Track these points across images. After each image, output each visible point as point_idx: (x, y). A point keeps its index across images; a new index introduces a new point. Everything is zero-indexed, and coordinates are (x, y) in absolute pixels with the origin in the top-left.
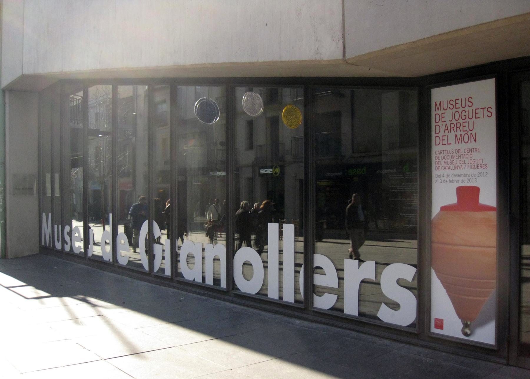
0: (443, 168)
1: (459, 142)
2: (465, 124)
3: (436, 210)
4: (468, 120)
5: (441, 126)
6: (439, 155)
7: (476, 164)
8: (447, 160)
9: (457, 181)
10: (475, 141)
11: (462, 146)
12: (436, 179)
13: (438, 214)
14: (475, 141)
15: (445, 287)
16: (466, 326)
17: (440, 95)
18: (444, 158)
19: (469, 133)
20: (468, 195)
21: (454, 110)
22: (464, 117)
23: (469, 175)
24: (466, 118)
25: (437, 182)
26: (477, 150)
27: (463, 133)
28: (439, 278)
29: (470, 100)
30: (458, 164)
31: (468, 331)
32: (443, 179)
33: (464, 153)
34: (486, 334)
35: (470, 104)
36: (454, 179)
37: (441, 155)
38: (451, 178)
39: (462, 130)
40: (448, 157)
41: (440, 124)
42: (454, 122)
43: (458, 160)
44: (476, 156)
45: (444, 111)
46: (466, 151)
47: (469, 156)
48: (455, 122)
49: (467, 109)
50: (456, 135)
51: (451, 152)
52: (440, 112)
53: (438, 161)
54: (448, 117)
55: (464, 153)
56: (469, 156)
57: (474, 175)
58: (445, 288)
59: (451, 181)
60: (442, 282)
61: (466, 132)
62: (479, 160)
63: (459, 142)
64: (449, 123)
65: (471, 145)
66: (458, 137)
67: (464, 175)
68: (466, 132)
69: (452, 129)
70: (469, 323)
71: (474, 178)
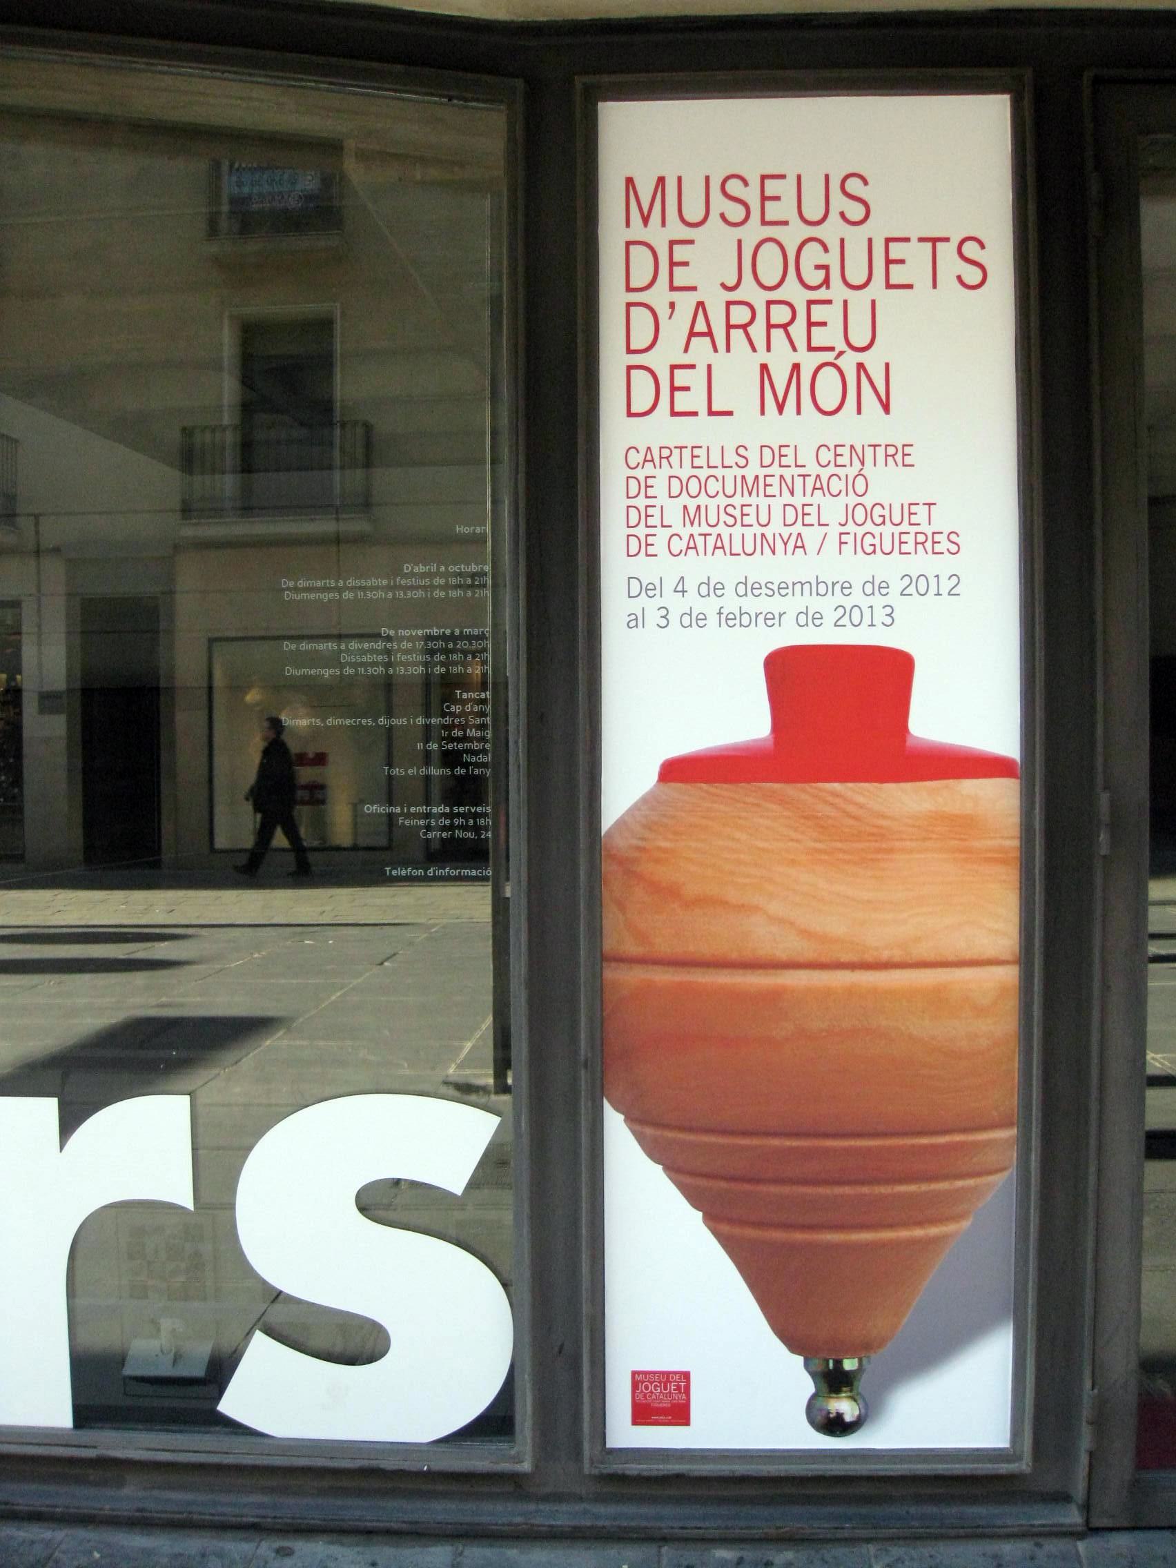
0: (677, 545)
1: (781, 408)
2: (818, 313)
3: (627, 779)
4: (837, 291)
5: (663, 312)
6: (649, 469)
7: (888, 529)
8: (703, 500)
9: (771, 619)
10: (886, 408)
11: (802, 431)
12: (635, 606)
13: (647, 801)
14: (886, 408)
15: (695, 1198)
16: (834, 1380)
17: (646, 140)
18: (684, 487)
19: (849, 362)
20: (839, 708)
21: (753, 232)
22: (815, 278)
23: (846, 587)
24: (826, 282)
25: (635, 621)
26: (899, 454)
27: (809, 362)
28: (655, 1150)
29: (854, 186)
30: (776, 527)
31: (845, 1407)
32: (677, 605)
33: (813, 469)
34: (960, 1403)
35: (856, 212)
36: (752, 605)
37: (665, 471)
38: (731, 603)
39: (801, 343)
40: (713, 486)
41: (659, 296)
42: (749, 291)
43: (776, 504)
44: (888, 486)
45: (687, 233)
46: (826, 456)
47: (850, 486)
48: (759, 299)
49: (832, 231)
50: (764, 368)
51: (731, 458)
52: (658, 236)
53: (641, 502)
54: (710, 260)
55: (813, 469)
56: (850, 486)
57: (882, 588)
58: (696, 1205)
59: (726, 619)
60: (674, 1170)
61: (829, 357)
62: (909, 510)
63: (781, 408)
64: (716, 304)
65: (862, 426)
66: (780, 381)
67: (819, 587)
68: (829, 357)
69: (737, 335)
70: (849, 1365)
71: (878, 601)
